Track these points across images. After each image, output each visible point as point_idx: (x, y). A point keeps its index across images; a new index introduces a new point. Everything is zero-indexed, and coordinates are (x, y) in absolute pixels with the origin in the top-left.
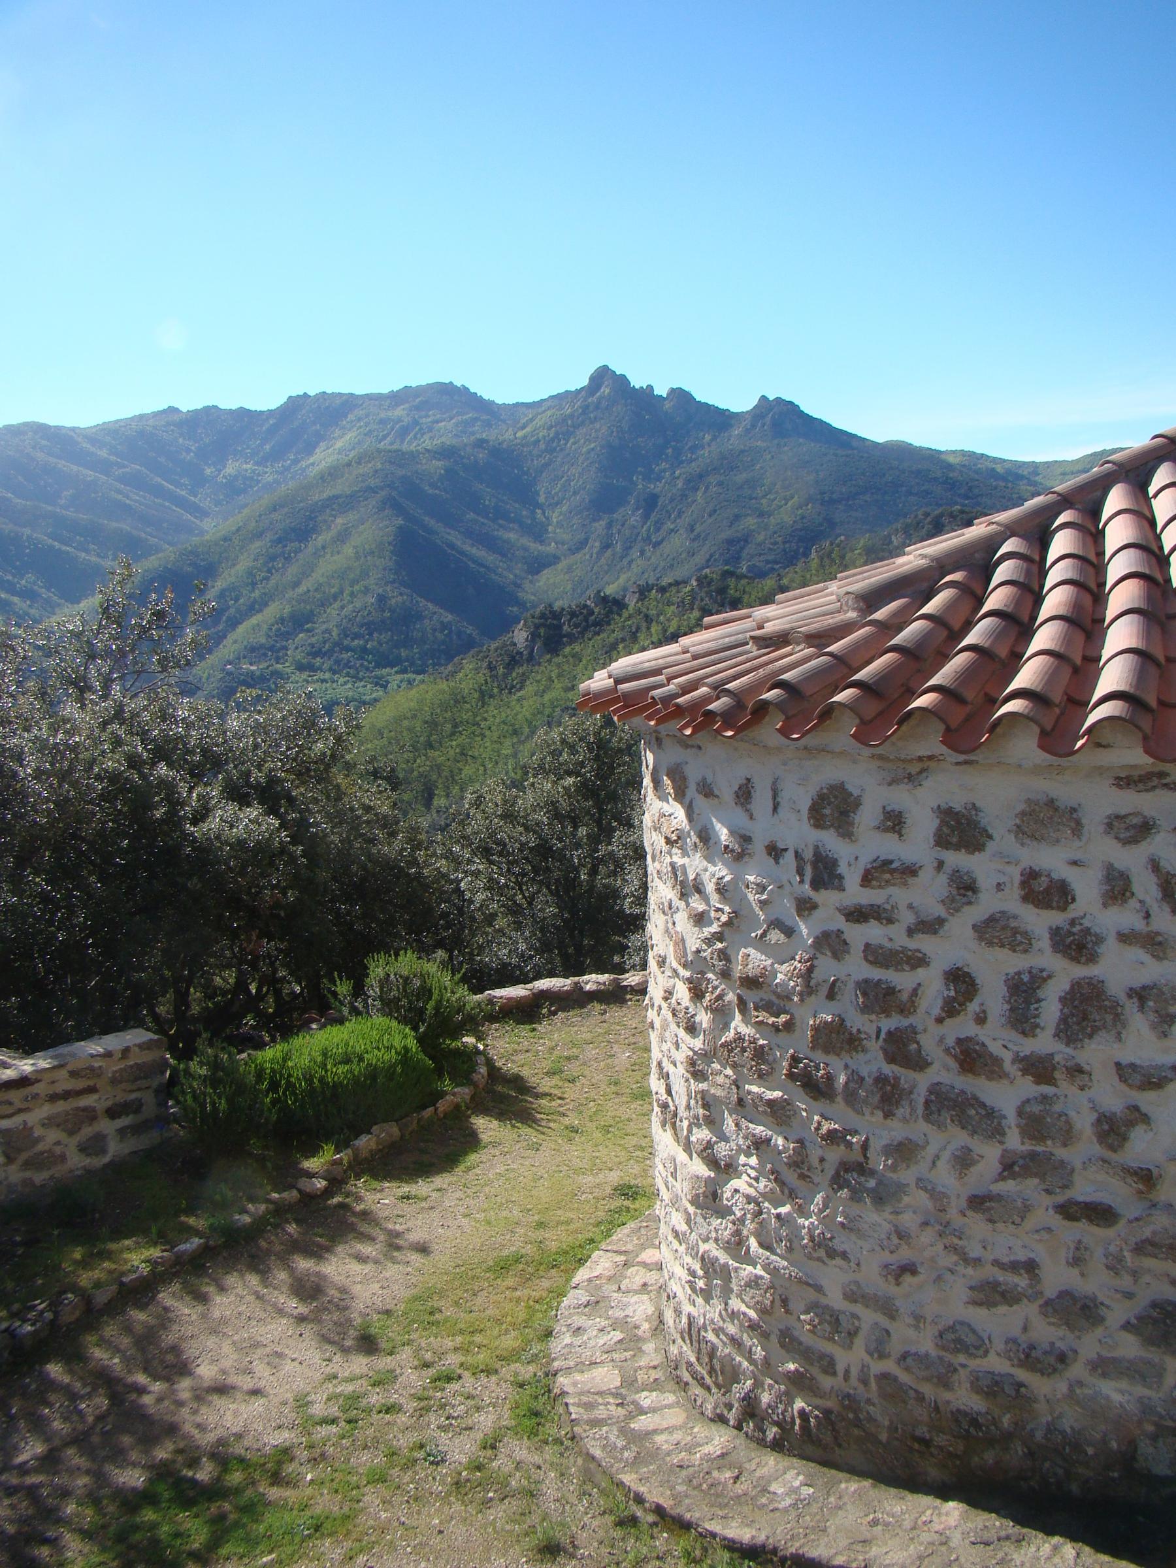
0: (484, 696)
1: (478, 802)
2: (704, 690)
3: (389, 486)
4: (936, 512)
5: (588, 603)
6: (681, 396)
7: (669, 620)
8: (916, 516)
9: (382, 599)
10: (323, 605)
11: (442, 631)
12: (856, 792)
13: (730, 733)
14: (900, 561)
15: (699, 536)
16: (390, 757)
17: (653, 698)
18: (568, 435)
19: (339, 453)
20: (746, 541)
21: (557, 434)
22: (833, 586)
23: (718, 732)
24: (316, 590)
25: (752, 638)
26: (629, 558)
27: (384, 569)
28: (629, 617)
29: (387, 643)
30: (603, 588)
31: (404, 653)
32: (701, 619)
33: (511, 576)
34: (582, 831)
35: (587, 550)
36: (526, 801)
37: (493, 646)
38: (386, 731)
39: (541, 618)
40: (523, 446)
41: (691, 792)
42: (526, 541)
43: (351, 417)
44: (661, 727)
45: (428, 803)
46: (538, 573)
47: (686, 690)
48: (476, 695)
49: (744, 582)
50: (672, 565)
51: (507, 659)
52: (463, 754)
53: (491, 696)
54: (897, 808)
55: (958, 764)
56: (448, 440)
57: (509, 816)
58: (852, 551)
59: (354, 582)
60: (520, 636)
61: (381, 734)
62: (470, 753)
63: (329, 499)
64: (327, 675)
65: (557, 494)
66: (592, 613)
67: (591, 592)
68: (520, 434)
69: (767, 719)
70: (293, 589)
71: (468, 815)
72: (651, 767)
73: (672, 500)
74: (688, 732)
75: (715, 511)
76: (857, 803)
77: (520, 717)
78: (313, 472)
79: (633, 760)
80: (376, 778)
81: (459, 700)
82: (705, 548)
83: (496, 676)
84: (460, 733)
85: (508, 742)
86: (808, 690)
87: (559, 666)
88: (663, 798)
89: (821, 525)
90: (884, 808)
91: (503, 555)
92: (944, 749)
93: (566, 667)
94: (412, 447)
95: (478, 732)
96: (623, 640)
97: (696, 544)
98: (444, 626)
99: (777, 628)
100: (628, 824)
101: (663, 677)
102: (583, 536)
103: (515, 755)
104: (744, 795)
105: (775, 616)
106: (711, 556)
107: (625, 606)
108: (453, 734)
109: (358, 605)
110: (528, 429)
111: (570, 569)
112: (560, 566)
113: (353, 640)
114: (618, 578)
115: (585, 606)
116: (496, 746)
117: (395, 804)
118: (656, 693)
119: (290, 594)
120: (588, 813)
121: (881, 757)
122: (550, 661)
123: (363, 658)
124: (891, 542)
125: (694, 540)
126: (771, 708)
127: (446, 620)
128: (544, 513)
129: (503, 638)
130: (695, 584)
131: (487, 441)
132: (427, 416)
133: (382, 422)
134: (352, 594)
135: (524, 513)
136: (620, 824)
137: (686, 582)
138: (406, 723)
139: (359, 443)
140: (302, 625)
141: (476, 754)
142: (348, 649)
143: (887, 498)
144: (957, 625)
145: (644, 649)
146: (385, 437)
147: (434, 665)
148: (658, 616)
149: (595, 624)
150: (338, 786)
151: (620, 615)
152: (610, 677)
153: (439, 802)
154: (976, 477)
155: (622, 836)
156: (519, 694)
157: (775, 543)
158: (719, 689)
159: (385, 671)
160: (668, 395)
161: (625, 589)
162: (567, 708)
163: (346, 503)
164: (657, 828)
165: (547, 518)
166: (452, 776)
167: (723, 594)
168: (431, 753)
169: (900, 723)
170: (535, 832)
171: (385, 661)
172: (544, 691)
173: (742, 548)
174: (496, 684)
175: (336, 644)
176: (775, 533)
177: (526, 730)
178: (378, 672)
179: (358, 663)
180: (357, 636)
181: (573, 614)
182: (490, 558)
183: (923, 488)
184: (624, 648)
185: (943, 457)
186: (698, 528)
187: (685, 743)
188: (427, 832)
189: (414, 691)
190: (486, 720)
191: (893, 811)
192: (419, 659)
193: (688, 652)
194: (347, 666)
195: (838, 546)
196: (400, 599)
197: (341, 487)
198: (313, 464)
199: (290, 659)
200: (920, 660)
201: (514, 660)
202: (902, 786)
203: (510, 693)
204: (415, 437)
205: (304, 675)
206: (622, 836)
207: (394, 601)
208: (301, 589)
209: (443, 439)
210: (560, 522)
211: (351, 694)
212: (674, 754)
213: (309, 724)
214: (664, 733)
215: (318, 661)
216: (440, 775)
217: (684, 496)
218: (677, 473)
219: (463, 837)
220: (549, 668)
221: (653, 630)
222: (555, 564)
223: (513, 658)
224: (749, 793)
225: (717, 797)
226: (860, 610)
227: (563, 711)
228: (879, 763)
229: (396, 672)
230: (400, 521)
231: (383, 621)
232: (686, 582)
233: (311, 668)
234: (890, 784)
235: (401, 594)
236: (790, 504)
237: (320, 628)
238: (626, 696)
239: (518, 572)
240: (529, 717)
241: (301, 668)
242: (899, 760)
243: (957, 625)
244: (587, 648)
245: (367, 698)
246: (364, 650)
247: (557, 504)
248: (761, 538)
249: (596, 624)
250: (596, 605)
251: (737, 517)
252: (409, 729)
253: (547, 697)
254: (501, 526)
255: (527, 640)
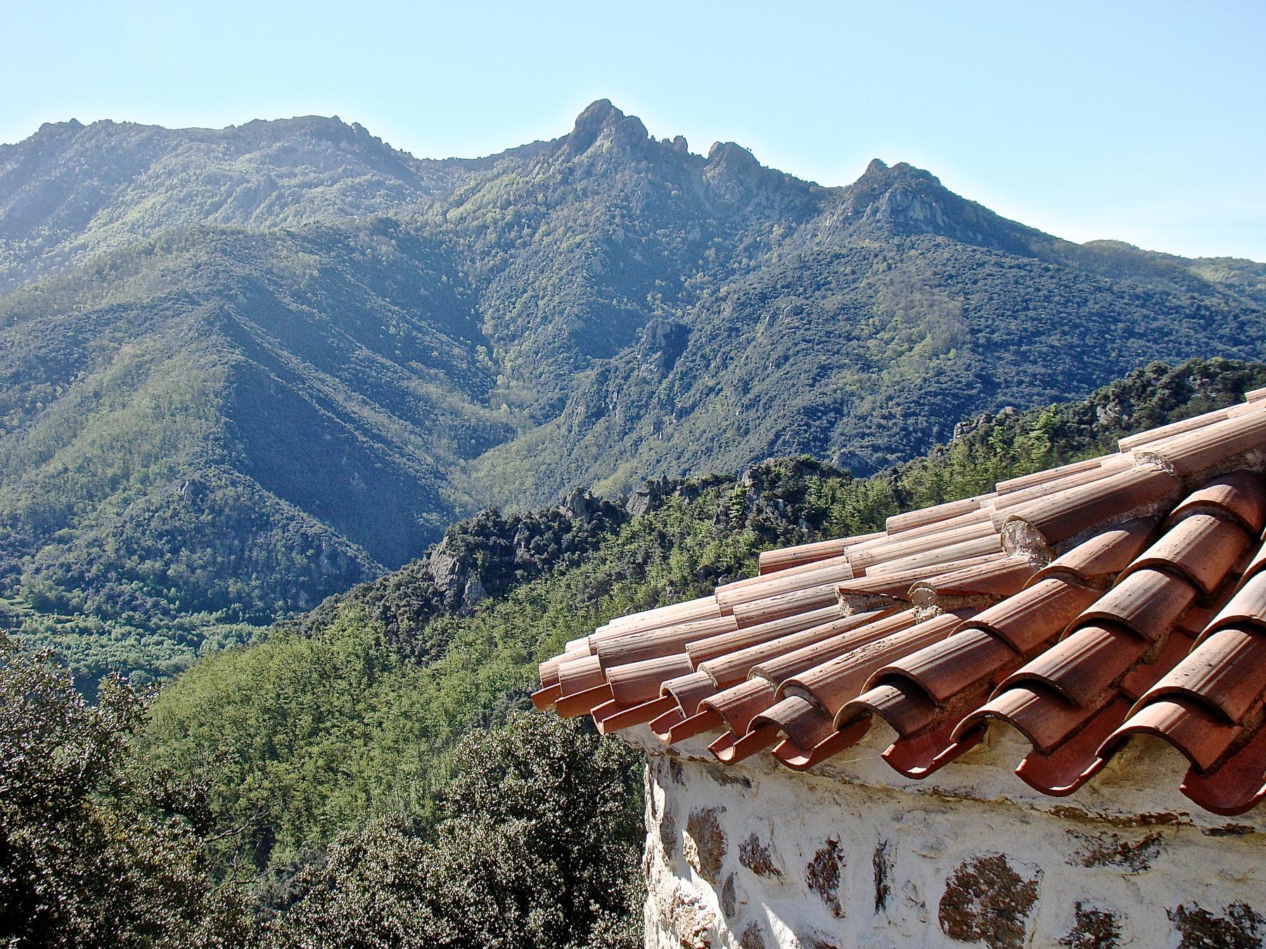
0: (373, 667)
1: (354, 859)
2: (756, 682)
3: (219, 292)
4: (1180, 367)
5: (562, 510)
6: (734, 158)
7: (701, 545)
8: (1141, 374)
9: (199, 490)
10: (91, 497)
11: (303, 552)
12: (1026, 876)
13: (801, 761)
14: (1109, 462)
15: (757, 399)
16: (198, 771)
17: (667, 692)
18: (536, 219)
19: (132, 230)
20: (839, 411)
21: (518, 215)
22: (989, 503)
23: (781, 757)
24: (80, 469)
25: (842, 591)
26: (634, 436)
27: (206, 439)
28: (633, 537)
29: (203, 570)
30: (589, 485)
31: (233, 587)
32: (753, 550)
33: (430, 460)
34: (536, 918)
35: (561, 419)
36: (439, 859)
37: (393, 580)
38: (194, 723)
39: (478, 534)
40: (456, 234)
41: (731, 861)
42: (458, 400)
43: (155, 168)
44: (679, 746)
45: (262, 859)
46: (476, 455)
47: (725, 680)
48: (359, 665)
49: (833, 481)
50: (710, 450)
51: (416, 604)
52: (329, 769)
53: (386, 668)
54: (1102, 909)
55: (1214, 832)
56: (328, 218)
57: (406, 887)
58: (1025, 432)
59: (148, 460)
60: (441, 564)
61: (185, 730)
62: (343, 768)
63: (111, 309)
64: (92, 622)
65: (514, 320)
66: (568, 528)
67: (567, 492)
68: (453, 214)
69: (867, 738)
70: (38, 466)
71: (333, 880)
72: (660, 814)
73: (713, 338)
74: (727, 755)
75: (786, 358)
76: (1029, 896)
77: (434, 706)
78: (83, 261)
79: (629, 790)
80: (169, 812)
81: (328, 673)
82: (768, 422)
83: (396, 633)
84: (327, 731)
85: (411, 750)
86: (942, 690)
87: (506, 618)
88: (680, 871)
89: (970, 386)
90: (1078, 906)
91: (416, 422)
92: (1189, 805)
93: (518, 621)
94: (264, 228)
95: (360, 729)
96: (620, 576)
97: (752, 414)
98: (308, 542)
99: (887, 577)
100: (619, 908)
101: (686, 656)
102: (557, 394)
103: (423, 774)
104: (825, 871)
105: (885, 554)
106: (777, 436)
107: (625, 518)
108: (314, 732)
109: (156, 499)
110: (468, 206)
111: (531, 451)
112: (514, 446)
113: (142, 559)
114: (615, 469)
115: (557, 515)
116: (390, 756)
117: (201, 859)
118: (674, 684)
119: (31, 474)
120: (548, 884)
121: (1072, 814)
122: (491, 609)
123: (159, 594)
124: (1094, 418)
125: (747, 408)
126: (875, 719)
127: (310, 532)
128: (490, 352)
129: (411, 566)
130: (748, 482)
131: (396, 224)
132: (292, 175)
133: (212, 180)
134: (145, 480)
135: (456, 351)
136: (603, 907)
137: (731, 480)
138: (230, 711)
139: (169, 214)
140: (48, 531)
141: (354, 769)
142: (132, 576)
143: (1089, 341)
144: (1210, 576)
145: (653, 601)
146: (217, 206)
147: (286, 609)
148: (683, 536)
149: (572, 547)
150: (97, 826)
151: (616, 534)
152: (593, 651)
153: (283, 854)
154: (1253, 306)
155: (606, 930)
156: (439, 664)
157: (891, 416)
158: (783, 682)
159: (196, 618)
160: (711, 154)
161: (627, 489)
162: (518, 693)
163: (143, 319)
164: (668, 925)
165: (496, 362)
166: (308, 809)
167: (795, 508)
168: (273, 766)
169: (1107, 754)
170: (453, 917)
171: (197, 600)
172: (479, 662)
173: (832, 424)
174: (395, 646)
175: (110, 566)
176: (890, 398)
177: (445, 730)
178: (186, 619)
179: (150, 602)
180: (149, 554)
181: (534, 530)
182: (394, 427)
183: (1155, 325)
184: (622, 590)
185: (1193, 270)
186: (757, 388)
187: (721, 774)
188: (257, 910)
189: (247, 656)
190: (374, 709)
191: (1095, 913)
192: (261, 598)
193: (730, 613)
194: (130, 604)
195: (1000, 423)
196: (231, 491)
197: (133, 290)
198: (84, 247)
199: (24, 590)
200: (1143, 642)
201: (427, 609)
202: (1111, 868)
203: (419, 663)
204: (270, 211)
205: (49, 620)
206: (606, 930)
207: (219, 494)
208: (53, 466)
209: (319, 217)
210: (518, 372)
211: (133, 656)
212: (701, 793)
213: (49, 710)
214: (684, 755)
215: (76, 596)
216: (286, 807)
217: (733, 331)
218: (724, 290)
219: (321, 924)
220: (488, 621)
221: (673, 561)
222: (505, 440)
223: (427, 601)
224: (835, 868)
225: (778, 873)
226: (1036, 549)
227: (510, 697)
228: (1068, 824)
229: (218, 620)
230: (237, 356)
231: (199, 530)
232: (731, 480)
233: (63, 607)
234: (1089, 864)
235: (233, 483)
236: (917, 348)
237: (83, 538)
238: (619, 685)
239: (441, 453)
240: (451, 707)
241: (43, 606)
242: (1106, 820)
243: (1210, 576)
244: (559, 589)
245: (162, 664)
246: (162, 578)
247: (513, 338)
248: (865, 407)
249: (578, 547)
250: (575, 515)
251: (824, 370)
252: (234, 722)
253: (483, 673)
254: (413, 371)
255: (452, 571)
